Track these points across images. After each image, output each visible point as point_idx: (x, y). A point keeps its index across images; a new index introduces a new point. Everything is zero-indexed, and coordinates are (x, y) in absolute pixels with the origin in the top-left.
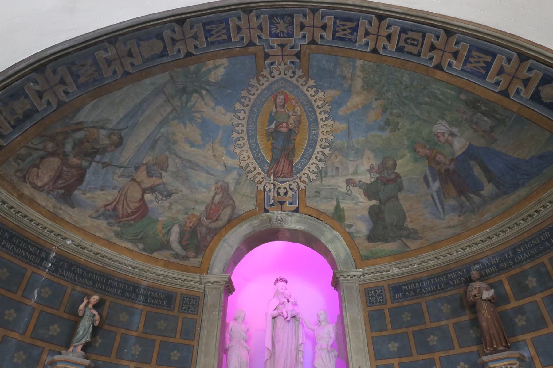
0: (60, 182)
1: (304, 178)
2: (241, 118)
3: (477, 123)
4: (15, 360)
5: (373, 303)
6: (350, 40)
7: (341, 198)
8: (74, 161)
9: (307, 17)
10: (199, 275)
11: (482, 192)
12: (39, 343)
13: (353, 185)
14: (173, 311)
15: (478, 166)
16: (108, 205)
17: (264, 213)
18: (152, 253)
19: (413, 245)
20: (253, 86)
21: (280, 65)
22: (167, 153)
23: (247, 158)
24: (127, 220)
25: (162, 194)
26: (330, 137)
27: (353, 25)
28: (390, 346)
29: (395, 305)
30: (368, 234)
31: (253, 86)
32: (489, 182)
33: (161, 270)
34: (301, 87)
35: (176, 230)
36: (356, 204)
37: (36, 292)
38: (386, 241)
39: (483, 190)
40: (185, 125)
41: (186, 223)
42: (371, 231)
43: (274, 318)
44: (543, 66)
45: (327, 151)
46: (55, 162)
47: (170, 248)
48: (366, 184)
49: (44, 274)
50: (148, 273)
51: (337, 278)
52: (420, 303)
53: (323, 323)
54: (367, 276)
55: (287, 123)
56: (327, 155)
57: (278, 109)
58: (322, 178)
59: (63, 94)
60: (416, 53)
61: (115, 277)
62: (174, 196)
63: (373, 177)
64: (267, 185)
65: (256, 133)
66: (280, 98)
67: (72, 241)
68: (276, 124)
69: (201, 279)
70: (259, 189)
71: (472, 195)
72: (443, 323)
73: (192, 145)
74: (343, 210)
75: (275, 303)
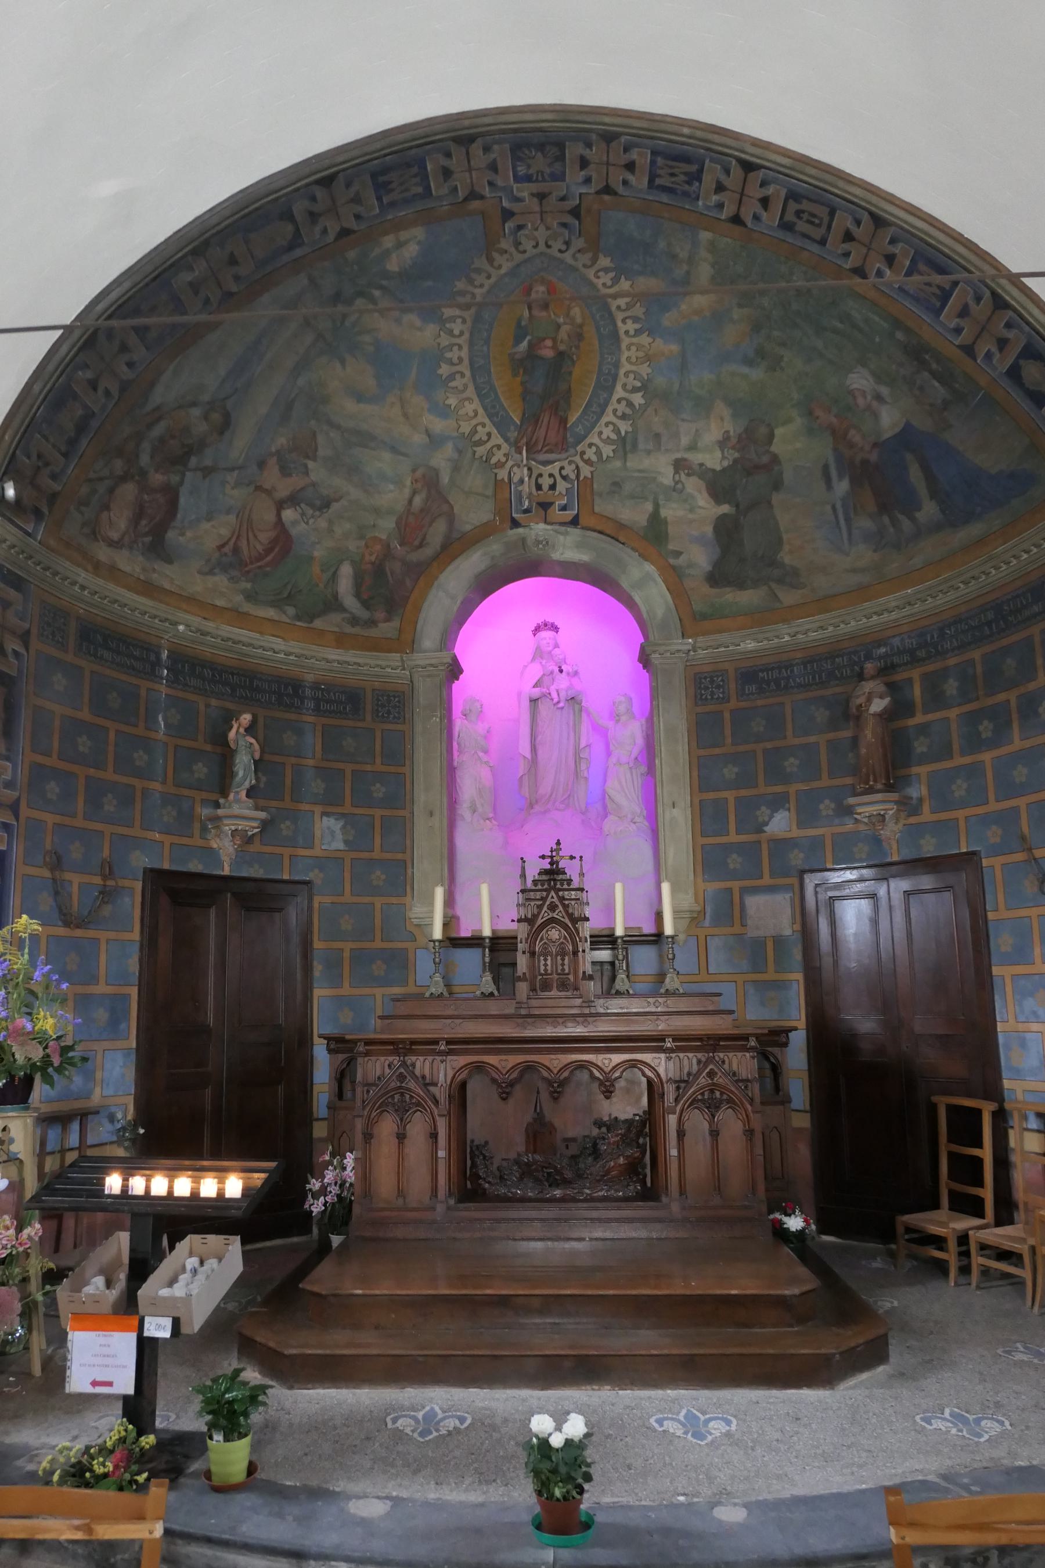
0: (144, 522)
1: (590, 454)
2: (456, 332)
3: (921, 388)
4: (165, 819)
5: (706, 699)
6: (686, 194)
7: (661, 497)
8: (157, 478)
9: (594, 148)
10: (399, 655)
11: (918, 515)
12: (186, 792)
13: (686, 471)
14: (364, 720)
15: (917, 465)
16: (223, 546)
17: (511, 529)
18: (311, 622)
19: (789, 597)
20: (478, 271)
21: (536, 229)
22: (313, 422)
23: (471, 414)
24: (260, 567)
25: (312, 506)
26: (645, 370)
27: (694, 168)
28: (725, 771)
29: (743, 704)
30: (710, 571)
31: (478, 271)
32: (931, 498)
33: (334, 654)
34: (583, 270)
35: (346, 570)
36: (692, 510)
37: (160, 718)
38: (741, 585)
39: (919, 510)
40: (343, 362)
41: (363, 556)
42: (717, 565)
43: (534, 701)
44: (1027, 328)
45: (638, 399)
46: (129, 491)
47: (340, 608)
48: (714, 471)
49: (163, 689)
50: (313, 661)
51: (648, 655)
52: (783, 704)
53: (624, 718)
54: (700, 651)
55: (554, 340)
56: (637, 407)
57: (536, 312)
58: (625, 454)
59: (125, 368)
60: (818, 237)
61: (262, 673)
62: (335, 506)
63: (726, 458)
64: (515, 469)
65: (489, 362)
66: (537, 292)
67: (187, 626)
68: (530, 342)
69: (402, 661)
70: (499, 478)
71: (900, 517)
72: (812, 739)
73: (360, 397)
74: (665, 522)
75: (535, 672)
